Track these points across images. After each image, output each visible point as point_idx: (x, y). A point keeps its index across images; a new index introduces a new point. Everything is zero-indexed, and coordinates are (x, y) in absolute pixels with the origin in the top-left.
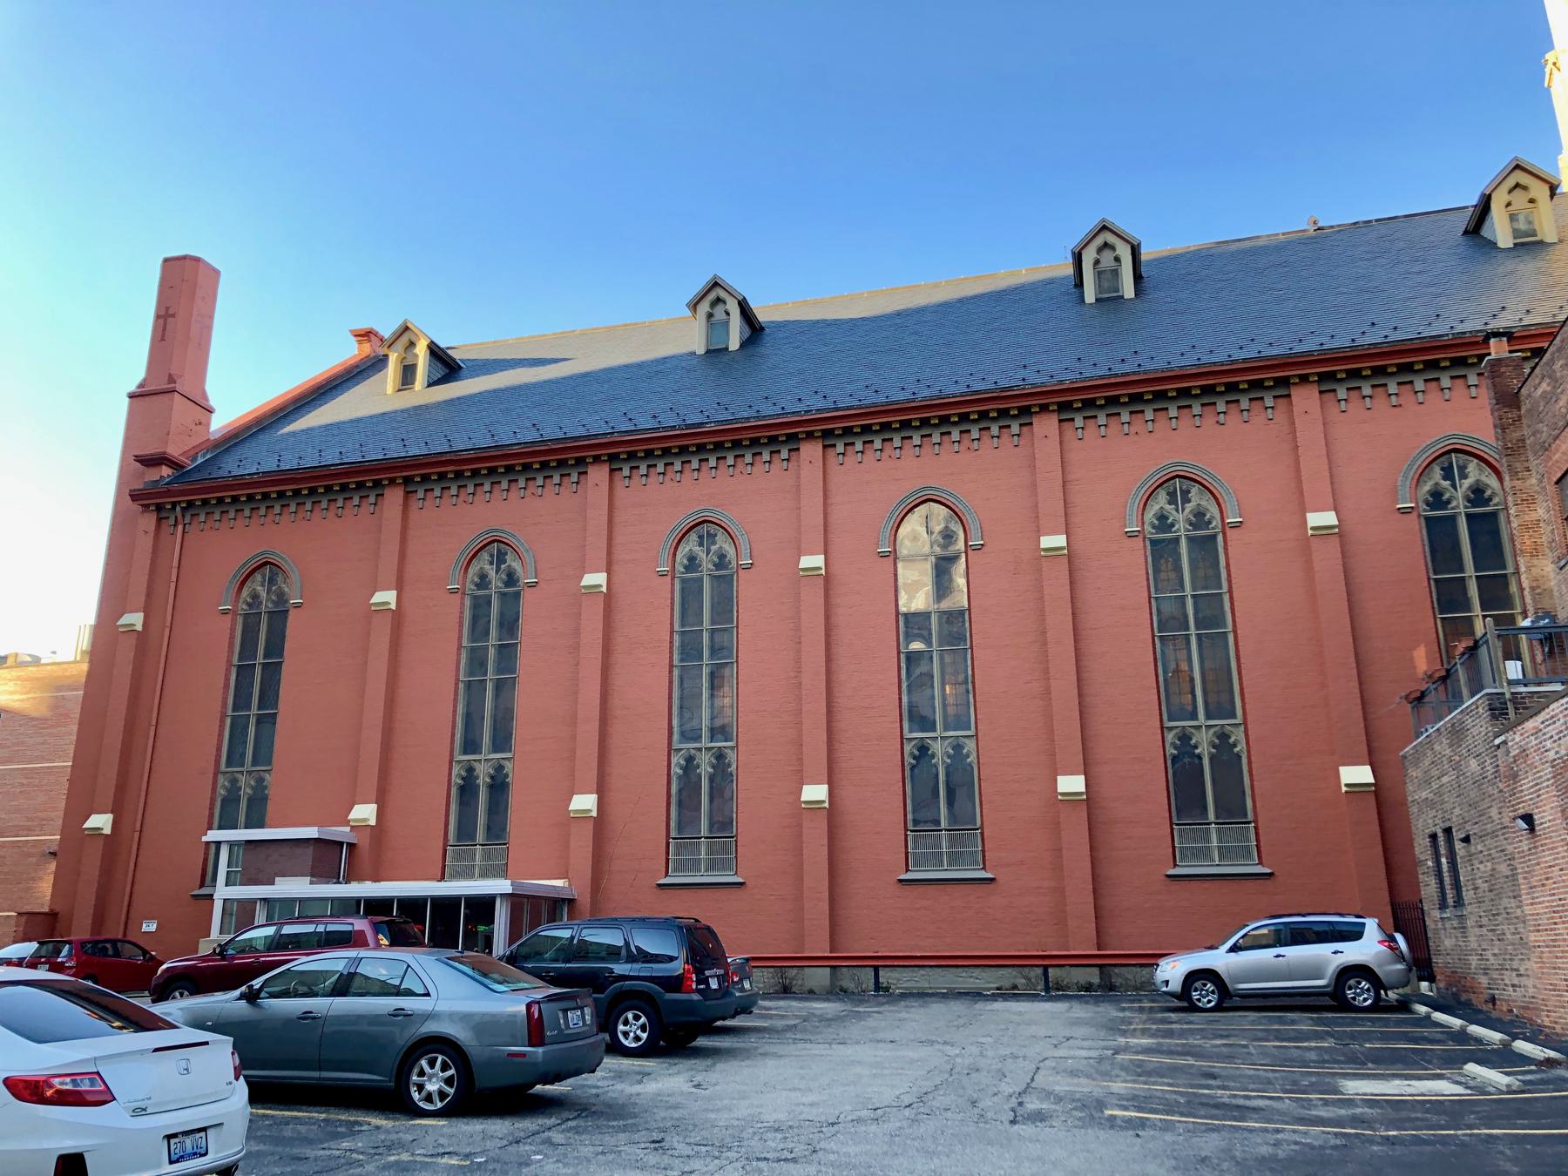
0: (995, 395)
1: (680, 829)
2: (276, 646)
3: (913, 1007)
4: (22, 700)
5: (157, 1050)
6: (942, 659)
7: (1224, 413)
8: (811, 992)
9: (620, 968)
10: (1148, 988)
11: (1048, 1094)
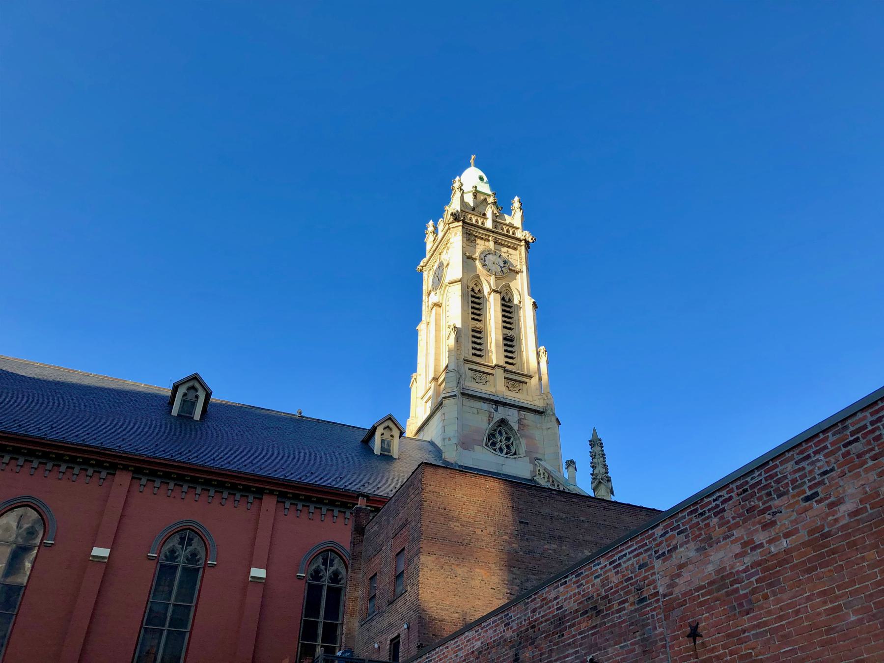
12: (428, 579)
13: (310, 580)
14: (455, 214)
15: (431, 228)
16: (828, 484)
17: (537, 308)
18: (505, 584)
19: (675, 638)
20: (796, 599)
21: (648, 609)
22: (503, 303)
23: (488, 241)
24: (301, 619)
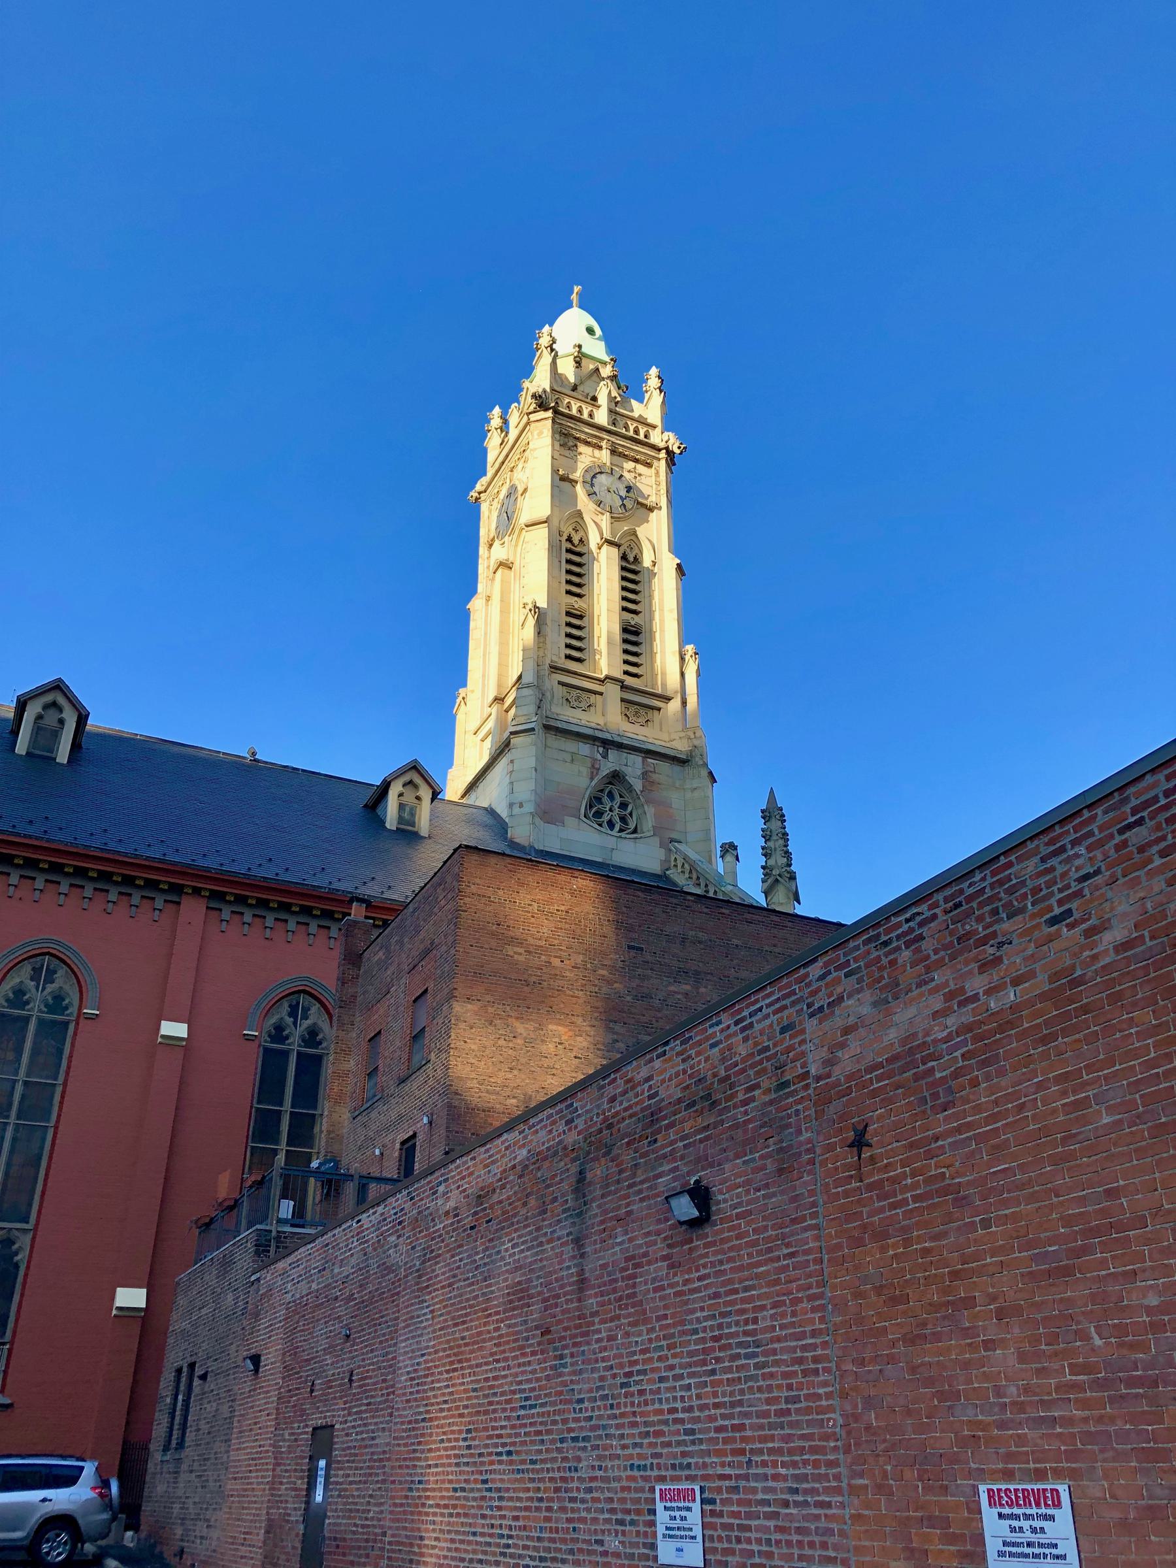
7: (114, 902)
12: (465, 1042)
13: (266, 1041)
14: (540, 396)
15: (496, 422)
16: (1088, 895)
17: (683, 574)
18: (598, 1049)
19: (830, 1148)
20: (1020, 1087)
21: (791, 1100)
22: (624, 564)
23: (600, 448)
24: (251, 1107)
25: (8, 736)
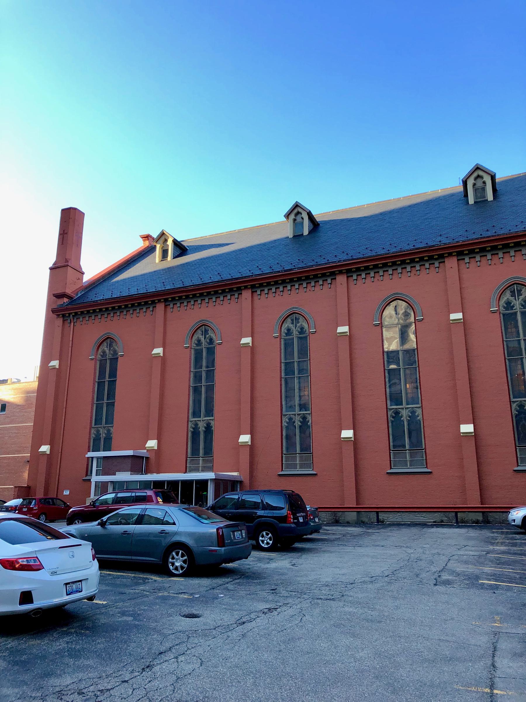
0: (427, 249)
1: (287, 449)
2: (113, 373)
3: (393, 530)
4: (14, 398)
5: (60, 548)
6: (405, 371)
8: (348, 523)
9: (260, 513)
10: (506, 523)
11: (452, 572)
25: (464, 198)
